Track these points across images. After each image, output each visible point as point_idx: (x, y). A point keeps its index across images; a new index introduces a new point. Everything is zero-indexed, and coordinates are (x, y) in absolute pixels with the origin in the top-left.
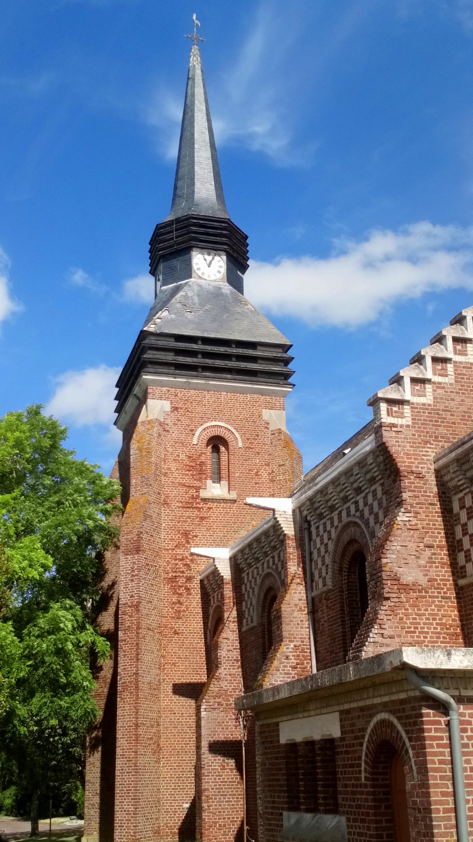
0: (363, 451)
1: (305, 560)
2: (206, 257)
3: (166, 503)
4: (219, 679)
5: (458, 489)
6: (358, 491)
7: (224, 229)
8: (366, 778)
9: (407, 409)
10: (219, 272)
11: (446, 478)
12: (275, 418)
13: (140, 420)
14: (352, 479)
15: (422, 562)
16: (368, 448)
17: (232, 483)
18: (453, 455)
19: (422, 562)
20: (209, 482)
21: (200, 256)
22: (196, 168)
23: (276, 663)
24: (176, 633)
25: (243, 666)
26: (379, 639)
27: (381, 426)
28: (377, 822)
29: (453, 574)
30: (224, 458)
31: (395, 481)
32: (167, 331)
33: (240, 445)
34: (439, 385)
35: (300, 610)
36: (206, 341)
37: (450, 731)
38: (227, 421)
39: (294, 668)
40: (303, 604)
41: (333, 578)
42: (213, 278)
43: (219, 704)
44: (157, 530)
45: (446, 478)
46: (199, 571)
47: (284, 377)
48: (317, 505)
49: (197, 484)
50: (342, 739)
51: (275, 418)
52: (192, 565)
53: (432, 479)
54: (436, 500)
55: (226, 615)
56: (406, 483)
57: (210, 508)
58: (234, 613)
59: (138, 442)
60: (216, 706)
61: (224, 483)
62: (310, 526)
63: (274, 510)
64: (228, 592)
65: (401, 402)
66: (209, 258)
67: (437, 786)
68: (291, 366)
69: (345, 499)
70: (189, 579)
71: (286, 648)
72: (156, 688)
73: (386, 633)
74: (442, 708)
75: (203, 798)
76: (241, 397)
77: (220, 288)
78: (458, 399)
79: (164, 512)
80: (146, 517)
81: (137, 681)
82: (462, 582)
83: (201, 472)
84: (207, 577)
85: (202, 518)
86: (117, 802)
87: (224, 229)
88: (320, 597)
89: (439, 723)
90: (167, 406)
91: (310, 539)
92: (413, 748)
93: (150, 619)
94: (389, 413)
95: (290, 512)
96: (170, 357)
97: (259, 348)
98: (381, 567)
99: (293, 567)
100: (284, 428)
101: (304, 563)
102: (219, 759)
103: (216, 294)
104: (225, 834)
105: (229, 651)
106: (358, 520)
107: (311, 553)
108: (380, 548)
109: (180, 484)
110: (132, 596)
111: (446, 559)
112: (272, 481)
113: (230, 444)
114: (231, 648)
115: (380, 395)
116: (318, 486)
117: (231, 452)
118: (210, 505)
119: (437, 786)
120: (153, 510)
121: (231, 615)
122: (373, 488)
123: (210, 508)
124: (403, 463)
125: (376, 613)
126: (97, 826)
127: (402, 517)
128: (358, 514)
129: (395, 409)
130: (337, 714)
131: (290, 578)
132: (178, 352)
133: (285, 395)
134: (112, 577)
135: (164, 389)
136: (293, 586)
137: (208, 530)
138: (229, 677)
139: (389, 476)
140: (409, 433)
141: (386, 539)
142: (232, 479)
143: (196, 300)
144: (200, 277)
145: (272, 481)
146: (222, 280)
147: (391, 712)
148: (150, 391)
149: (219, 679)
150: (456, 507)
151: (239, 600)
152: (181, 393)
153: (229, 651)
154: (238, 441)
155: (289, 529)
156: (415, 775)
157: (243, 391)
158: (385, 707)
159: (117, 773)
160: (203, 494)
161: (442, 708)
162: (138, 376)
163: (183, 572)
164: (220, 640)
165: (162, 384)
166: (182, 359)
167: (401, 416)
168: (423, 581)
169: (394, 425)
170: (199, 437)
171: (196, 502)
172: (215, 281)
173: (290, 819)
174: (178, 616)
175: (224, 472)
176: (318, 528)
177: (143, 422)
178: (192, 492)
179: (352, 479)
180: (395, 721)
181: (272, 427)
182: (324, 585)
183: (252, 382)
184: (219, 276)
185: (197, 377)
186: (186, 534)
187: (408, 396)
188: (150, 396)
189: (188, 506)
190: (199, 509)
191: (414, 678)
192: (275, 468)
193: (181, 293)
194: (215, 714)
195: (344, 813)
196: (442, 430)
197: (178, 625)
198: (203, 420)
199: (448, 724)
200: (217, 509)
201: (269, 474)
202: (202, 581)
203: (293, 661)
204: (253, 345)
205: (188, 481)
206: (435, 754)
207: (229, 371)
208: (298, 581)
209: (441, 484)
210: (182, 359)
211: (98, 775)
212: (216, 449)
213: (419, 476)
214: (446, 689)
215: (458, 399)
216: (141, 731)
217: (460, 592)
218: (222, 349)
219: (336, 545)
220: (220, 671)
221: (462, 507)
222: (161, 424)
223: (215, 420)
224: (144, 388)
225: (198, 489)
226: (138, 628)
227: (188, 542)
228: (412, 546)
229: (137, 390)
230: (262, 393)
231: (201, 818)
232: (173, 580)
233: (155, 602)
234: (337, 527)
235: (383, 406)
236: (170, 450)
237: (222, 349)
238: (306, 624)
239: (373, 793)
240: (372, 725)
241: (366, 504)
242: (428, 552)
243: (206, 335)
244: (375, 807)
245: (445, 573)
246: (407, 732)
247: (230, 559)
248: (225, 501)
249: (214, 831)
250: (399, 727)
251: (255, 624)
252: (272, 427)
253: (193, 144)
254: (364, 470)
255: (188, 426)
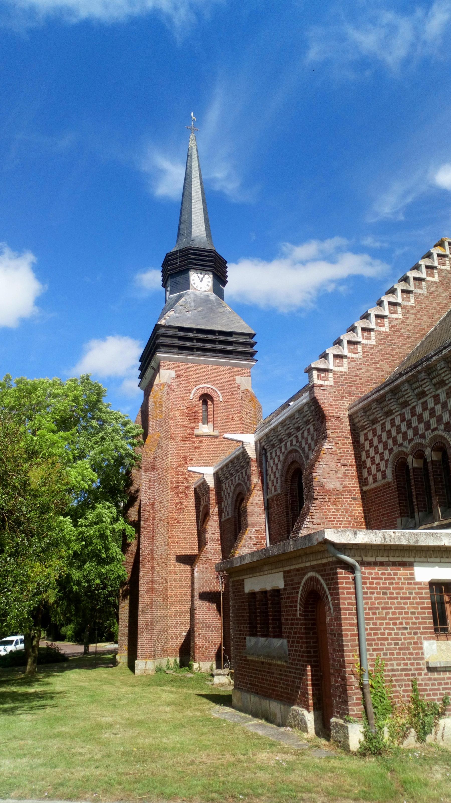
0: (302, 403)
1: (263, 475)
2: (199, 275)
3: (172, 438)
4: (206, 552)
5: (363, 428)
6: (298, 429)
7: (212, 257)
8: (300, 614)
9: (330, 375)
10: (208, 285)
11: (356, 421)
12: (244, 382)
13: (155, 383)
14: (294, 421)
15: (340, 475)
16: (304, 401)
17: (216, 425)
18: (360, 405)
19: (340, 475)
20: (200, 424)
21: (195, 275)
22: (193, 216)
23: (243, 541)
24: (178, 522)
25: (222, 544)
26: (310, 525)
27: (313, 386)
28: (307, 643)
29: (360, 483)
30: (210, 408)
31: (322, 422)
32: (173, 324)
33: (221, 399)
34: (352, 359)
35: (260, 507)
36: (199, 331)
37: (355, 584)
38: (213, 384)
39: (255, 544)
40: (261, 503)
41: (281, 487)
42: (204, 289)
43: (206, 568)
44: (166, 455)
45: (356, 421)
46: (194, 482)
47: (251, 355)
48: (271, 438)
49: (193, 425)
50: (285, 589)
51: (244, 382)
52: (189, 479)
53: (346, 421)
54: (349, 435)
55: (211, 511)
56: (329, 423)
57: (201, 441)
58: (217, 509)
59: (154, 397)
60: (204, 569)
61: (210, 425)
62: (266, 452)
63: (242, 442)
64: (213, 495)
65: (327, 371)
66: (201, 276)
67: (346, 619)
68: (255, 348)
69: (289, 435)
70: (187, 488)
71: (250, 532)
72: (165, 558)
73: (315, 521)
74: (351, 569)
75: (196, 629)
76: (222, 368)
77: (208, 296)
78: (364, 368)
79: (171, 444)
80: (159, 447)
81: (153, 554)
82: (365, 488)
83: (195, 417)
84: (199, 486)
85: (196, 448)
86: (139, 632)
87: (212, 257)
88: (272, 498)
89: (348, 578)
90: (173, 374)
91: (266, 461)
92: (331, 594)
93: (161, 514)
94: (319, 378)
95: (253, 443)
96: (175, 342)
97: (234, 336)
98: (312, 478)
99: (255, 479)
100: (250, 389)
101: (262, 476)
102: (206, 603)
103: (206, 300)
104: (209, 652)
105: (213, 534)
106: (297, 448)
107: (267, 470)
108: (312, 466)
109: (181, 425)
110: (149, 499)
111: (355, 473)
112: (242, 423)
113: (215, 399)
114: (214, 532)
115: (313, 366)
116: (272, 426)
117: (215, 405)
118: (201, 439)
119: (346, 619)
120: (163, 443)
121: (214, 510)
122: (308, 427)
123: (201, 441)
124: (327, 410)
125: (309, 508)
126: (126, 648)
127: (326, 446)
128: (298, 444)
129: (323, 375)
130: (282, 573)
131: (253, 486)
132: (181, 338)
133: (251, 367)
134: (137, 487)
135: (171, 363)
136: (255, 492)
137: (200, 455)
138: (213, 551)
139: (318, 419)
140: (332, 390)
141: (316, 459)
142: (215, 422)
143: (193, 304)
144: (195, 289)
145: (242, 423)
146: (209, 291)
147: (317, 571)
148: (161, 364)
149: (206, 552)
150: (362, 439)
151: (219, 501)
152: (182, 365)
153: (213, 534)
154: (219, 397)
155: (252, 454)
156: (332, 612)
157: (223, 364)
158: (313, 568)
159: (140, 613)
160: (197, 432)
161: (351, 569)
162: (154, 354)
163: (183, 483)
164: (207, 527)
165: (169, 360)
166: (183, 343)
167: (327, 379)
168: (340, 488)
169: (321, 386)
170: (194, 395)
171: (192, 437)
172: (205, 291)
173: (251, 641)
174: (180, 511)
175: (210, 418)
176: (271, 453)
177: (157, 385)
178: (189, 430)
179: (294, 421)
180: (320, 578)
181: (242, 388)
182: (275, 491)
183: (229, 358)
184: (208, 288)
185: (193, 355)
186: (185, 458)
187: (331, 366)
188: (161, 367)
189: (186, 440)
190: (194, 442)
191: (332, 549)
192: (244, 416)
193: (183, 299)
194: (203, 575)
195: (286, 637)
196: (354, 389)
197: (180, 517)
198: (197, 383)
199: (354, 579)
200: (206, 442)
201: (240, 419)
202: (195, 489)
203: (255, 540)
204: (230, 334)
205: (187, 423)
206: (345, 599)
207: (214, 351)
208: (258, 488)
209: (353, 424)
210: (183, 343)
211: (127, 615)
212: (205, 403)
213: (338, 419)
214: (353, 556)
215: (364, 368)
216: (155, 586)
217: (364, 495)
218: (209, 337)
219: (283, 465)
220: (207, 547)
221: (366, 439)
222: (169, 386)
223: (205, 383)
224: (158, 362)
225: (193, 428)
226: (154, 519)
227: (186, 463)
228: (333, 465)
229: (153, 363)
230: (236, 365)
231: (194, 642)
232: (177, 488)
233: (165, 502)
234: (284, 453)
235: (315, 373)
236: (175, 403)
237: (209, 337)
238: (263, 516)
239: (305, 624)
240: (304, 580)
241: (303, 438)
242: (343, 469)
243: (199, 327)
244: (306, 633)
245: (354, 483)
246: (327, 584)
247: (214, 474)
248: (210, 436)
249: (202, 650)
250: (322, 581)
251: (230, 516)
252: (242, 388)
253: (191, 200)
254: (302, 415)
255: (187, 387)
